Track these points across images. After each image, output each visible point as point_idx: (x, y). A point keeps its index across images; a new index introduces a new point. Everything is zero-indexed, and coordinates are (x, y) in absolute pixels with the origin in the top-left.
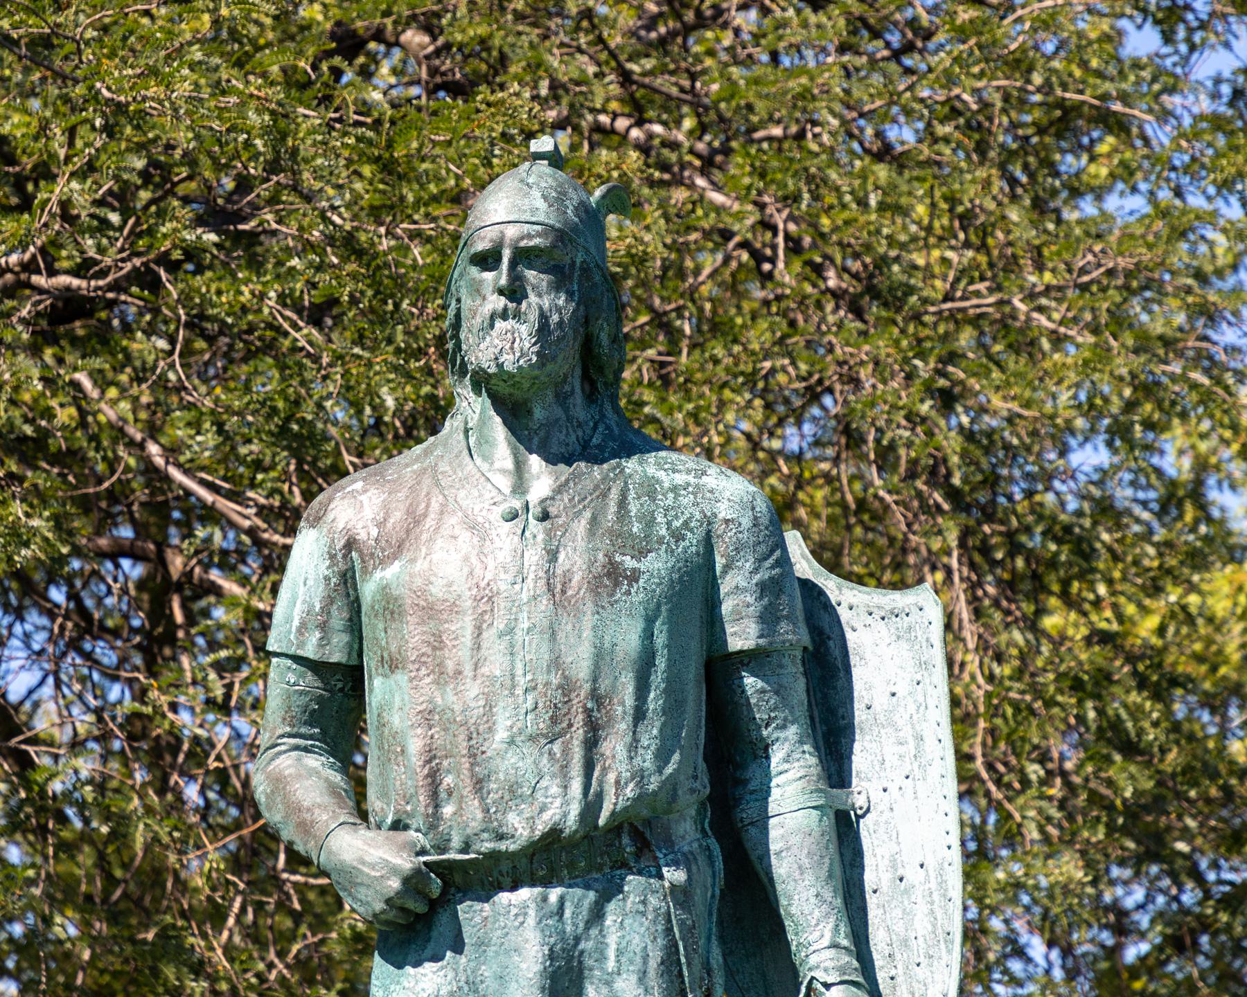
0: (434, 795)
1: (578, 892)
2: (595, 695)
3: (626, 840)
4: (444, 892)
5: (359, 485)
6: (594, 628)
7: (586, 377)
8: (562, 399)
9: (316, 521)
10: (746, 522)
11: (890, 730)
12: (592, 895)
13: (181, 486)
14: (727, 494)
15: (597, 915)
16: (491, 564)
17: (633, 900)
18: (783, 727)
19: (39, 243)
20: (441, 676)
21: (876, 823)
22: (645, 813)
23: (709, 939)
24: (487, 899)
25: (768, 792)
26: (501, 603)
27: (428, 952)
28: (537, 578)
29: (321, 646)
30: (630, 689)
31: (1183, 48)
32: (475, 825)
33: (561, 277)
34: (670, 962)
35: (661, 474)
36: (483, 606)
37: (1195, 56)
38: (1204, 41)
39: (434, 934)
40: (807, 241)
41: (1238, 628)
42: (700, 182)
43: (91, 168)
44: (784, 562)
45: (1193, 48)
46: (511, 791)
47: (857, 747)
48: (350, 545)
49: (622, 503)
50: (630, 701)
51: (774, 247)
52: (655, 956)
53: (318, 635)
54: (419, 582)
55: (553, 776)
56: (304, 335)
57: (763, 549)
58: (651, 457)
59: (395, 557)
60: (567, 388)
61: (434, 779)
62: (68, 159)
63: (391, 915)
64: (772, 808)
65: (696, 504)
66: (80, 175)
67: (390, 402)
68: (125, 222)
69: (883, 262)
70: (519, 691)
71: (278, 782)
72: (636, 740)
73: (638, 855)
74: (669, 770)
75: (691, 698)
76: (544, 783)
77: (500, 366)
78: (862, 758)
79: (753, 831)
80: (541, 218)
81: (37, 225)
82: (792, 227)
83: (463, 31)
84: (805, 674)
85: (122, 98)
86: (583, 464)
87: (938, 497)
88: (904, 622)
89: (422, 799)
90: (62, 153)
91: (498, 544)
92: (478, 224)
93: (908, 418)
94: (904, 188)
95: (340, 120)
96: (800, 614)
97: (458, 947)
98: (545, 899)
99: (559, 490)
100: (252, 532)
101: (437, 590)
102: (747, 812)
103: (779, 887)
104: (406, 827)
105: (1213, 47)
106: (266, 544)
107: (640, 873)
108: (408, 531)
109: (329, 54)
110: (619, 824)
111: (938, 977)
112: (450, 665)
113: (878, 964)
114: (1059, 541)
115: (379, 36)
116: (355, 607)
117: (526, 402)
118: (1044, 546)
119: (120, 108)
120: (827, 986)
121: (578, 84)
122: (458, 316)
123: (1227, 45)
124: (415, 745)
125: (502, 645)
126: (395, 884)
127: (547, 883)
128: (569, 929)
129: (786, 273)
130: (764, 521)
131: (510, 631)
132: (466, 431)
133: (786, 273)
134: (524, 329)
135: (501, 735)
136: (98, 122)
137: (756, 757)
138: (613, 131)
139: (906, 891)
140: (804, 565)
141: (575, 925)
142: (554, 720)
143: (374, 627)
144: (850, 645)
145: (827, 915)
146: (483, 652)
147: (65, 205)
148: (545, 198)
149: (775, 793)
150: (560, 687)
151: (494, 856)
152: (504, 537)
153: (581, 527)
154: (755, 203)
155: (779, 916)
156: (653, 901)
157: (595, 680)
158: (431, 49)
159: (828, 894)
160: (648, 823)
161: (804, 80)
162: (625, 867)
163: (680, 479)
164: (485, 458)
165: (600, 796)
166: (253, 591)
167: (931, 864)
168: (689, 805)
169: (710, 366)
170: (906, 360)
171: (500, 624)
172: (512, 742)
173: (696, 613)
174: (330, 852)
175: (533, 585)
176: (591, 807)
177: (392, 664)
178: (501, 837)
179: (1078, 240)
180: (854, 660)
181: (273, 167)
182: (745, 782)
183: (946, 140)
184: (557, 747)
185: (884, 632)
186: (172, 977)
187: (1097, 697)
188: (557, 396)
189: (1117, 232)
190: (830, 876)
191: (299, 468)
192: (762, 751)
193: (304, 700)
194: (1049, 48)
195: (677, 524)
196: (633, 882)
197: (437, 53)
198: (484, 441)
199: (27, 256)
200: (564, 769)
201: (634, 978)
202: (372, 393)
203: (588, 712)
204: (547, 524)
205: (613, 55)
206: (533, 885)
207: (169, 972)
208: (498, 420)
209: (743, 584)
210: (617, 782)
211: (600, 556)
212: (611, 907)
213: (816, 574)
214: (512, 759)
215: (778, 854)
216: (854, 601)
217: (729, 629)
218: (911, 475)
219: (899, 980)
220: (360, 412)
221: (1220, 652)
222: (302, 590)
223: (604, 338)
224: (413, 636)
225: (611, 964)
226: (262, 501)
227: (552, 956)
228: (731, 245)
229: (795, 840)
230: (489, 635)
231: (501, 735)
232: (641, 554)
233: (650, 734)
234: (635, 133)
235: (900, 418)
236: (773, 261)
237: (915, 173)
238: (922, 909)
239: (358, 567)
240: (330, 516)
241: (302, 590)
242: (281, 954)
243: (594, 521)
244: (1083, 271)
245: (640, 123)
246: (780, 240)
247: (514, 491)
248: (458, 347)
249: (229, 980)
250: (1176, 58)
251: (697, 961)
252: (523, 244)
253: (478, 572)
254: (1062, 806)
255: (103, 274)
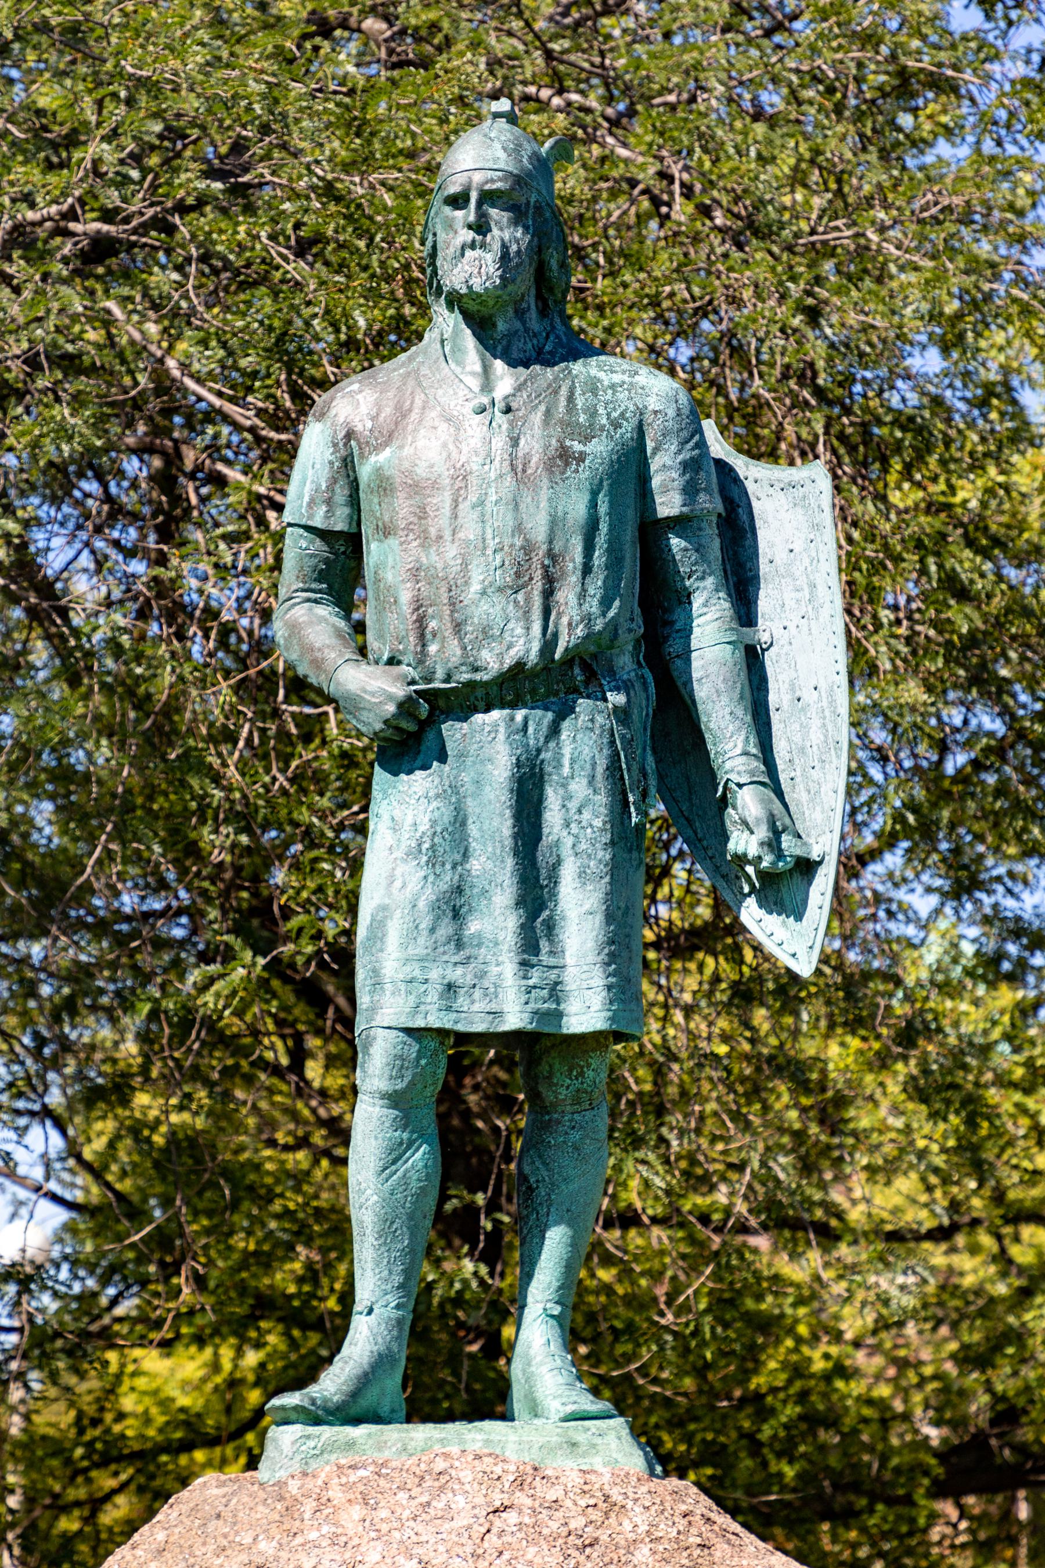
0: (422, 636)
1: (539, 712)
2: (551, 554)
3: (577, 671)
4: (431, 713)
5: (355, 387)
6: (550, 500)
7: (539, 296)
8: (520, 314)
9: (321, 417)
10: (671, 413)
11: (789, 580)
12: (550, 715)
13: (194, 393)
14: (655, 390)
15: (554, 731)
16: (465, 449)
17: (583, 718)
18: (703, 578)
19: (77, 193)
20: (425, 540)
21: (778, 655)
22: (592, 649)
23: (644, 749)
24: (465, 719)
25: (690, 631)
26: (473, 480)
27: (419, 762)
28: (502, 460)
29: (327, 518)
30: (579, 549)
31: (1002, 24)
32: (455, 660)
33: (519, 213)
34: (614, 768)
35: (601, 375)
36: (459, 483)
37: (1013, 30)
38: (1020, 18)
39: (423, 748)
40: (698, 187)
41: (1038, 501)
42: (610, 140)
43: (113, 135)
44: (702, 444)
45: (1010, 23)
46: (484, 632)
47: (762, 593)
48: (349, 435)
49: (571, 399)
50: (579, 559)
51: (671, 194)
52: (602, 764)
53: (324, 508)
54: (406, 465)
55: (518, 620)
56: (296, 268)
57: (685, 434)
58: (593, 361)
59: (386, 444)
60: (524, 305)
61: (421, 623)
62: (99, 124)
63: (389, 733)
64: (694, 644)
65: (630, 398)
66: (107, 139)
67: (362, 323)
68: (144, 178)
69: (760, 204)
70: (489, 552)
71: (294, 628)
72: (584, 590)
73: (587, 683)
74: (611, 613)
75: (628, 556)
76: (510, 626)
77: (470, 288)
78: (765, 603)
79: (678, 662)
80: (502, 165)
81: (75, 179)
82: (685, 176)
83: (417, 16)
84: (720, 535)
85: (144, 73)
86: (538, 367)
87: (806, 394)
88: (800, 492)
89: (412, 639)
90: (93, 119)
91: (470, 432)
92: (450, 171)
93: (782, 330)
94: (778, 142)
95: (320, 90)
96: (715, 487)
97: (443, 758)
98: (512, 719)
99: (519, 388)
100: (252, 430)
101: (421, 471)
102: (674, 647)
103: (700, 707)
104: (399, 663)
105: (1027, 23)
106: (265, 439)
107: (588, 697)
108: (397, 423)
109: (305, 37)
110: (572, 658)
111: (829, 777)
112: (433, 532)
113: (780, 767)
114: (904, 429)
115: (344, 25)
116: (354, 486)
117: (491, 317)
118: (891, 433)
119: (141, 82)
120: (740, 786)
121: (510, 58)
122: (434, 247)
123: (1037, 21)
124: (405, 597)
125: (475, 515)
126: (391, 708)
127: (513, 705)
128: (532, 742)
129: (681, 210)
130: (686, 411)
131: (481, 503)
132: (442, 341)
133: (681, 210)
134: (489, 257)
135: (475, 587)
136: (123, 94)
137: (680, 603)
138: (537, 100)
139: (803, 709)
140: (719, 447)
141: (537, 739)
142: (518, 575)
143: (371, 501)
144: (756, 512)
145: (739, 729)
146: (460, 521)
147: (96, 162)
148: (505, 149)
149: (696, 632)
150: (523, 548)
151: (471, 685)
152: (475, 427)
153: (537, 418)
154: (655, 157)
155: (700, 731)
156: (600, 719)
157: (551, 542)
158: (388, 33)
159: (740, 712)
160: (594, 656)
161: (695, 54)
162: (576, 691)
163: (617, 378)
164: (458, 363)
165: (556, 635)
166: (255, 477)
167: (823, 686)
168: (627, 641)
169: (621, 290)
170: (781, 283)
171: (473, 498)
172: (484, 593)
173: (632, 486)
174: (338, 684)
175: (499, 465)
176: (549, 645)
177: (386, 531)
178: (476, 669)
179: (920, 182)
180: (758, 523)
181: (265, 129)
182: (672, 623)
183: (811, 103)
184: (520, 597)
185: (783, 500)
186: (197, 787)
187: (938, 554)
188: (516, 311)
189: (952, 176)
190: (742, 698)
191: (289, 380)
192: (685, 598)
193: (314, 561)
194: (894, 25)
195: (615, 415)
196: (583, 705)
197: (392, 38)
198: (457, 349)
199: (65, 207)
200: (527, 613)
201: (585, 781)
202: (346, 315)
203: (546, 569)
204: (510, 416)
205: (537, 37)
206: (503, 708)
207: (194, 782)
208: (468, 332)
209: (669, 463)
210: (570, 624)
211: (554, 442)
212: (566, 724)
213: (727, 454)
214: (484, 606)
215: (699, 680)
216: (758, 476)
217: (658, 500)
218: (785, 376)
219: (798, 780)
220: (337, 331)
221: (1024, 520)
222: (310, 472)
223: (554, 264)
224: (402, 508)
225: (566, 771)
226: (260, 404)
227: (518, 764)
228: (636, 192)
229: (713, 669)
230: (464, 507)
231: (475, 587)
232: (587, 439)
233: (596, 585)
234: (556, 101)
235: (775, 329)
236: (669, 205)
237: (785, 130)
238: (816, 723)
239: (356, 452)
240: (333, 412)
241: (310, 472)
242: (283, 771)
243: (548, 413)
244: (923, 209)
245: (561, 91)
246: (677, 187)
247: (482, 390)
248: (435, 273)
249: (241, 790)
250: (997, 32)
251: (635, 767)
252: (487, 187)
253: (455, 455)
254: (908, 641)
255: (126, 220)
